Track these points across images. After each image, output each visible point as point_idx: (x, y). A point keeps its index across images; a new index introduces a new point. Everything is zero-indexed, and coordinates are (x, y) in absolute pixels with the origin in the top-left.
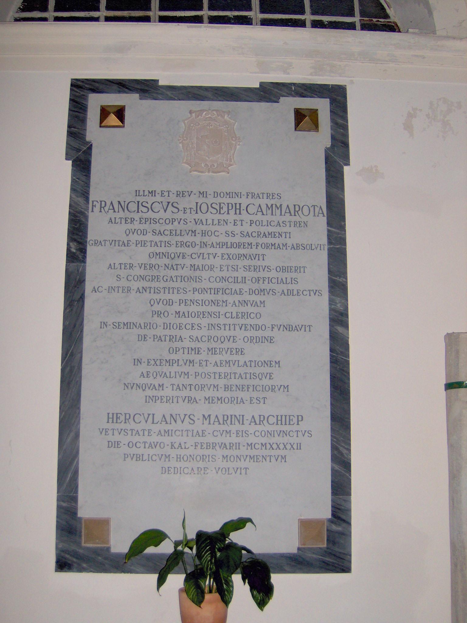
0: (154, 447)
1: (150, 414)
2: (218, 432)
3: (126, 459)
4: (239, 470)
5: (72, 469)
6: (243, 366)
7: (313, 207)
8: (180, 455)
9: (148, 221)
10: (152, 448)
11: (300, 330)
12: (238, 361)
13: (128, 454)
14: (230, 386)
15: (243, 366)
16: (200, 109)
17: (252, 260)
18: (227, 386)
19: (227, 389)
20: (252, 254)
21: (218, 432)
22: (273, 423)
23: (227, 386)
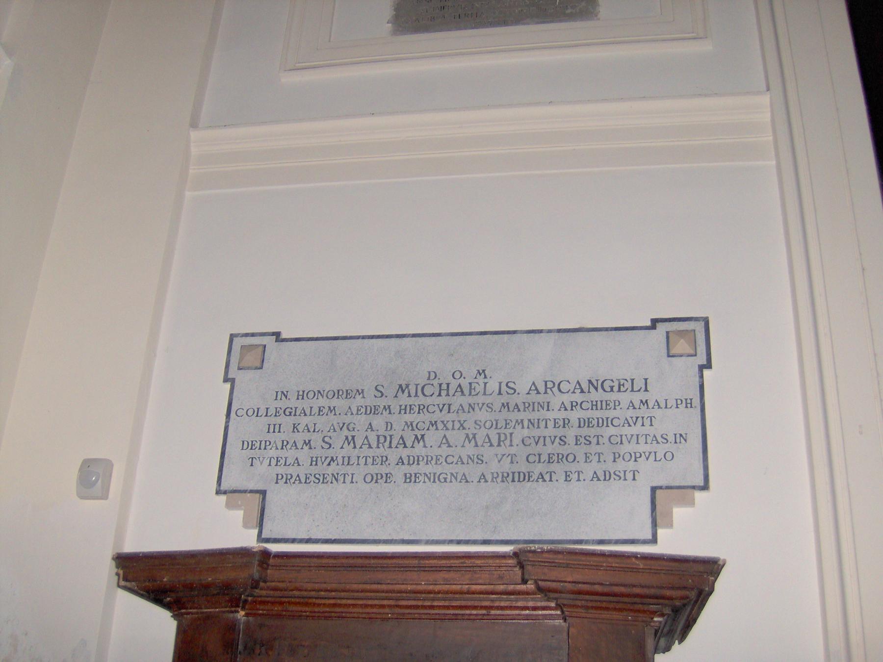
0: (633, 425)
1: (639, 417)
2: (535, 455)
3: (279, 481)
4: (640, 420)
5: (507, 562)
6: (293, 465)
7: (649, 418)
8: (687, 407)
9: (682, 403)
10: (630, 426)
11: (635, 424)
12: (655, 453)
13: (284, 475)
14: (413, 475)
15: (293, 465)
16: (281, 571)
17: (630, 426)
18: (408, 475)
19: (408, 480)
20: (631, 426)
21: (535, 455)
22: (534, 461)
23: (408, 475)
